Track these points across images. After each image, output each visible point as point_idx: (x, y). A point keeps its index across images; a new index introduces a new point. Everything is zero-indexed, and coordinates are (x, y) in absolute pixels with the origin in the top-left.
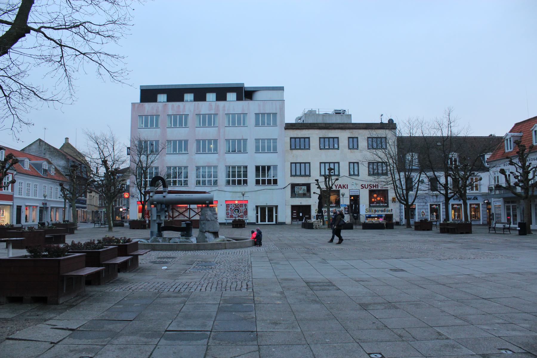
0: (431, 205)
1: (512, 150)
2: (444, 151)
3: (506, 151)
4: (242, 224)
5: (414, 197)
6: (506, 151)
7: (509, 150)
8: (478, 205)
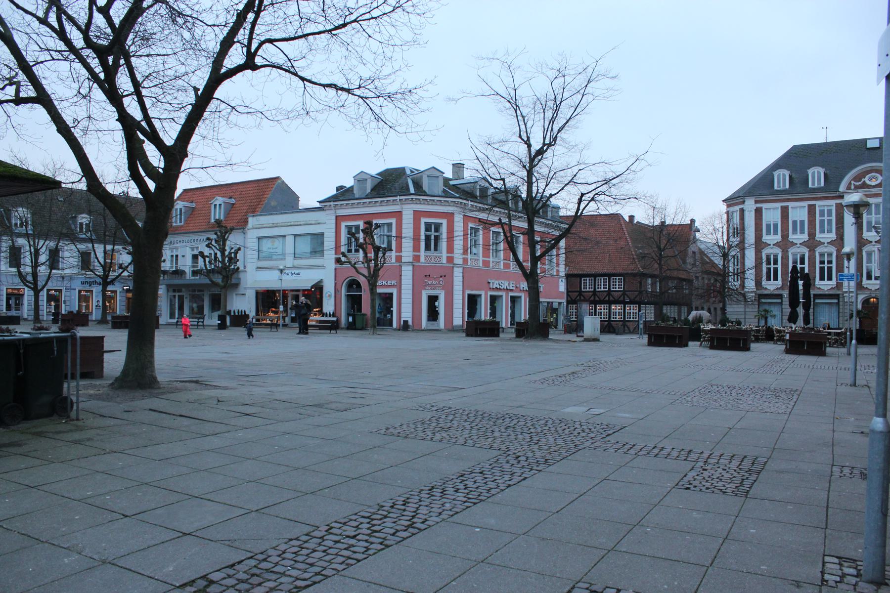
0: (80, 291)
1: (182, 224)
2: (104, 217)
3: (174, 224)
4: (739, 340)
5: (45, 279)
6: (174, 224)
7: (179, 224)
8: (115, 292)
